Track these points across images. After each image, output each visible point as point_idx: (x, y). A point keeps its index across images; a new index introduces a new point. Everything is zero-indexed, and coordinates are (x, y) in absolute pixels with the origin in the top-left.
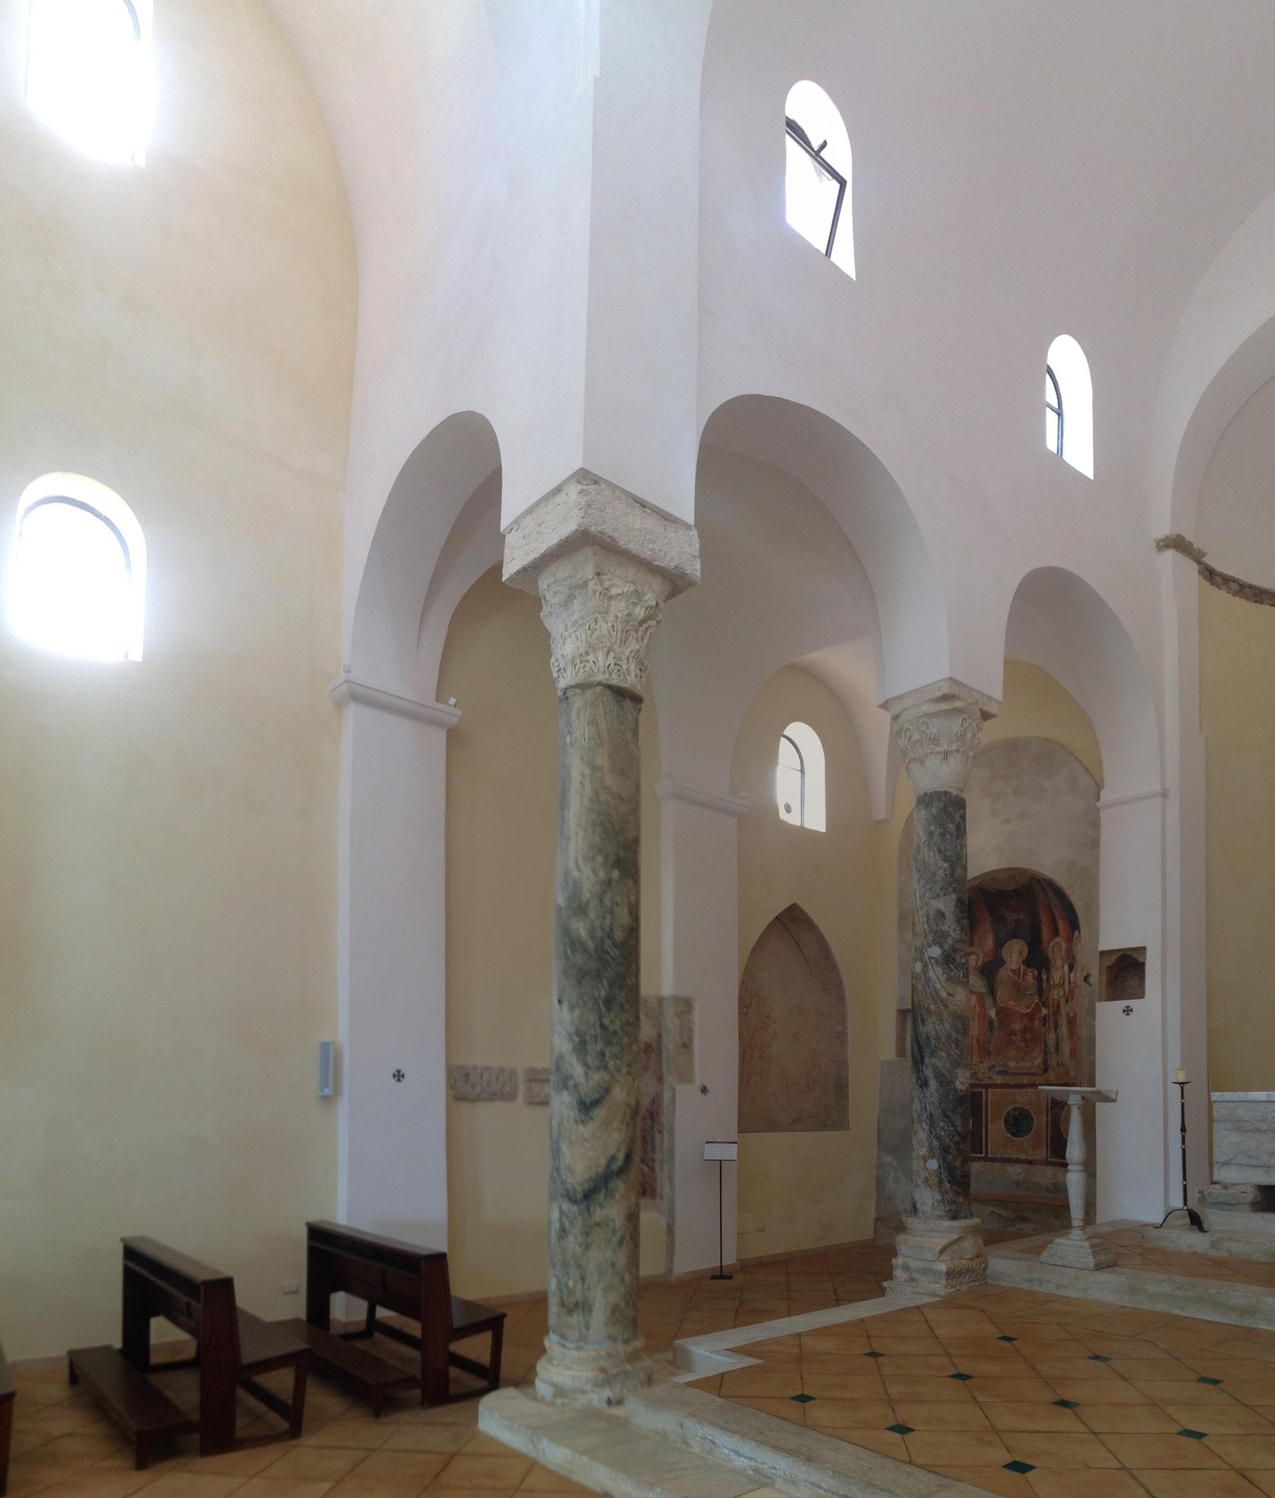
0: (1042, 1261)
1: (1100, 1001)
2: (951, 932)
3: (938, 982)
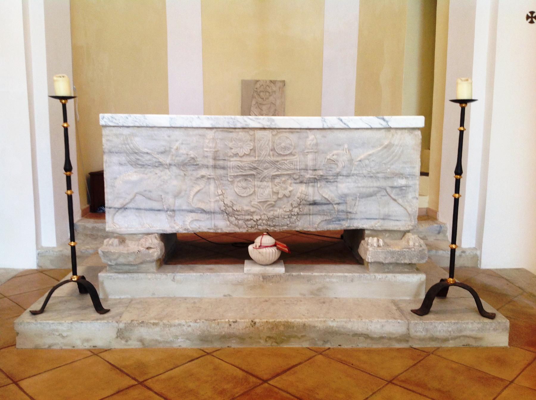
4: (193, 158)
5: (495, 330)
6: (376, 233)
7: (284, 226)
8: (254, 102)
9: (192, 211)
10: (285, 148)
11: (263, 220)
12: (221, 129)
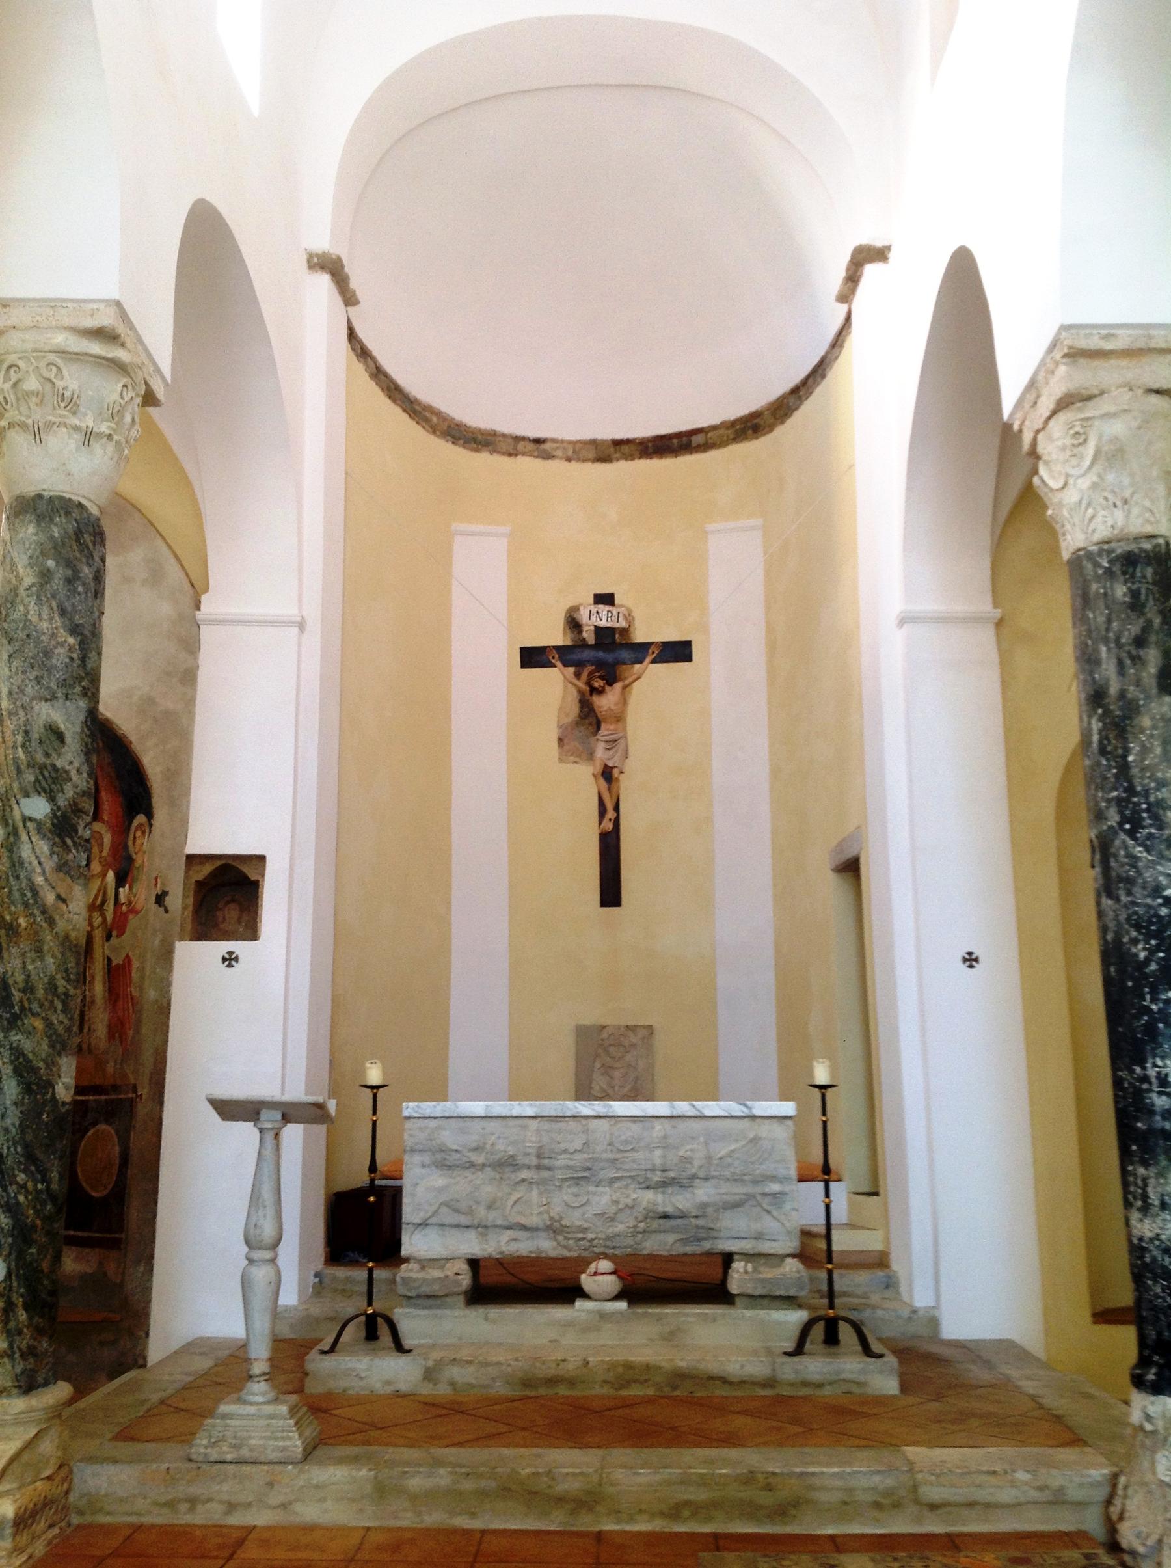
0: (194, 1457)
1: (181, 940)
2: (73, 773)
3: (39, 870)
4: (512, 1156)
5: (881, 1372)
6: (748, 1256)
7: (626, 1245)
8: (598, 1065)
9: (509, 1228)
10: (626, 1142)
11: (600, 1239)
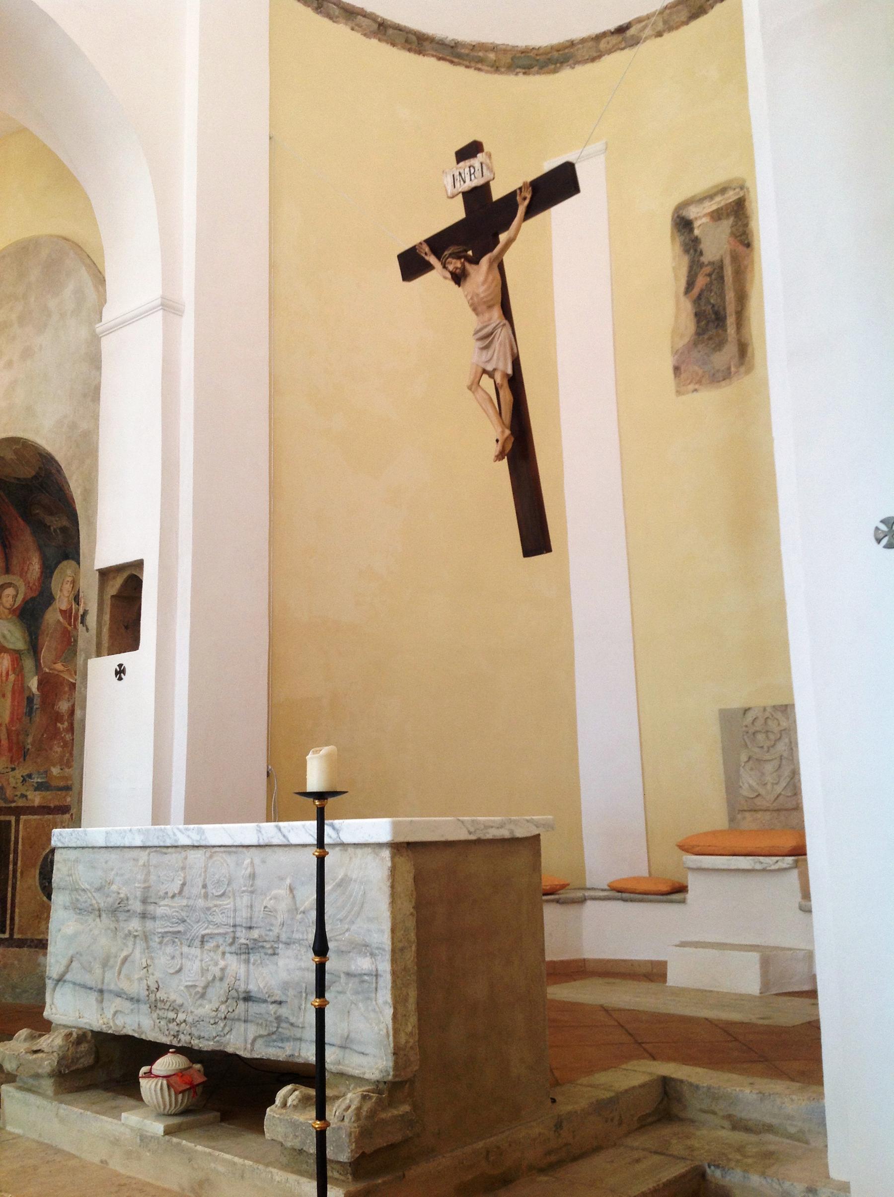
12: (155, 849)
